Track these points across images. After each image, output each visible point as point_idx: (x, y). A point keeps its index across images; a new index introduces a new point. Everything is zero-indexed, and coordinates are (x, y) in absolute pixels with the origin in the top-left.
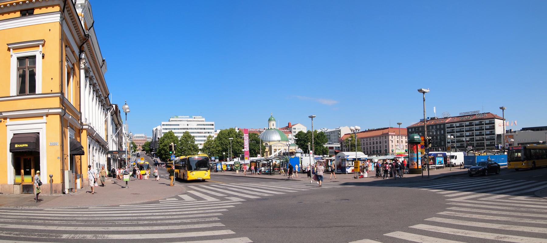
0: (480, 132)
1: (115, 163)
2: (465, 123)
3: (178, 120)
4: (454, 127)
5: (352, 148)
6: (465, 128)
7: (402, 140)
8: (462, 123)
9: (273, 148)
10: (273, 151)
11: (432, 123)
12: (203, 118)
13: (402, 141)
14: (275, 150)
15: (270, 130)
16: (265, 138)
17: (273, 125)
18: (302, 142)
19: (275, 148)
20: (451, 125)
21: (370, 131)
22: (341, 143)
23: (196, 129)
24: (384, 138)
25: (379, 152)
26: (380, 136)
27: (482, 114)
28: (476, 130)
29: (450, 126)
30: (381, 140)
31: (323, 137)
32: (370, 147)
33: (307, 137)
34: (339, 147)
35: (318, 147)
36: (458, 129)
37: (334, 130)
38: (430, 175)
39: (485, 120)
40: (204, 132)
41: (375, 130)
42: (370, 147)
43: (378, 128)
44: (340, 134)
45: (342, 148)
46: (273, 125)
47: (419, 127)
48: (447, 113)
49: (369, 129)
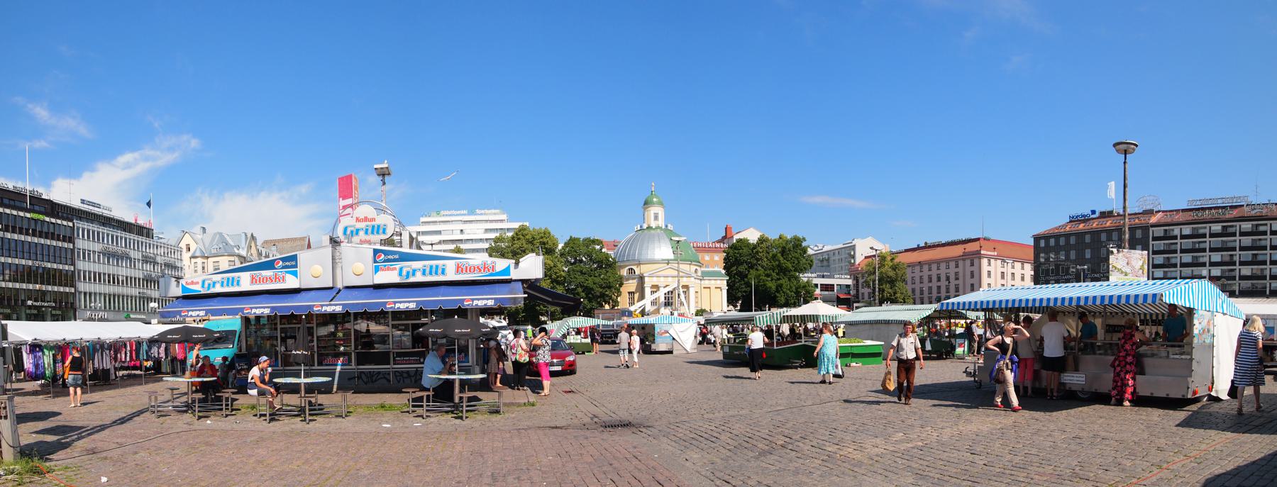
0: (1253, 254)
2: (1240, 226)
3: (440, 222)
4: (1175, 237)
5: (884, 286)
6: (1208, 242)
8: (1171, 227)
9: (648, 282)
10: (648, 291)
11: (1094, 225)
12: (504, 214)
13: (1013, 274)
14: (656, 288)
15: (646, 231)
16: (628, 255)
17: (656, 218)
18: (742, 268)
19: (655, 281)
20: (1166, 230)
21: (930, 247)
22: (856, 279)
23: (481, 240)
26: (956, 260)
27: (1264, 204)
28: (1242, 249)
29: (1162, 234)
30: (991, 269)
31: (799, 251)
32: (930, 288)
33: (757, 252)
34: (848, 286)
35: (784, 281)
36: (1188, 243)
37: (841, 246)
39: (1271, 222)
42: (930, 288)
44: (853, 257)
45: (858, 291)
46: (656, 218)
47: (1067, 236)
48: (1152, 198)
49: (926, 243)
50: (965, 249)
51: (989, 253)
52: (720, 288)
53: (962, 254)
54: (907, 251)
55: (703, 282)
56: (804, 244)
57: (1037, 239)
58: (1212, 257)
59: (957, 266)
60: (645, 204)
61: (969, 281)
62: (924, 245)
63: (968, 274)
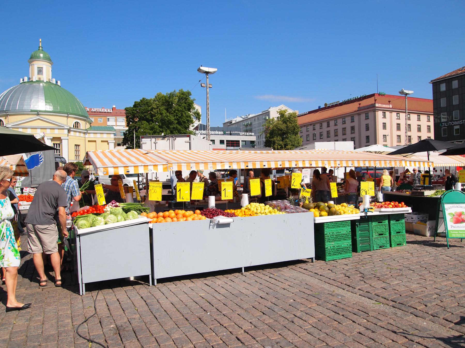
5: (275, 139)
17: (40, 71)
21: (329, 107)
24: (363, 116)
26: (352, 116)
30: (387, 121)
38: (440, 212)
41: (341, 104)
43: (346, 99)
49: (326, 104)
50: (360, 104)
51: (384, 106)
52: (107, 141)
53: (357, 109)
54: (310, 113)
55: (87, 136)
56: (192, 98)
57: (436, 84)
58: (427, 160)
59: (353, 121)
60: (31, 58)
61: (364, 134)
62: (324, 106)
63: (363, 128)
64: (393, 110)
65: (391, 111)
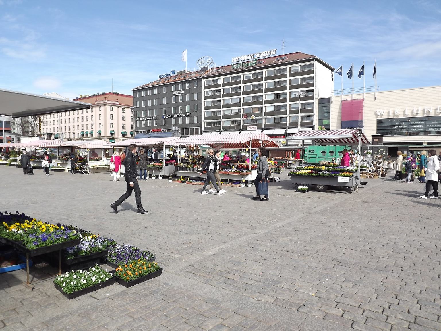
1: (421, 128)
7: (112, 113)
25: (89, 135)
39: (290, 66)
40: (53, 137)
43: (94, 94)
49: (81, 96)
63: (115, 117)
64: (119, 106)
65: (118, 106)
